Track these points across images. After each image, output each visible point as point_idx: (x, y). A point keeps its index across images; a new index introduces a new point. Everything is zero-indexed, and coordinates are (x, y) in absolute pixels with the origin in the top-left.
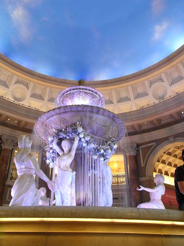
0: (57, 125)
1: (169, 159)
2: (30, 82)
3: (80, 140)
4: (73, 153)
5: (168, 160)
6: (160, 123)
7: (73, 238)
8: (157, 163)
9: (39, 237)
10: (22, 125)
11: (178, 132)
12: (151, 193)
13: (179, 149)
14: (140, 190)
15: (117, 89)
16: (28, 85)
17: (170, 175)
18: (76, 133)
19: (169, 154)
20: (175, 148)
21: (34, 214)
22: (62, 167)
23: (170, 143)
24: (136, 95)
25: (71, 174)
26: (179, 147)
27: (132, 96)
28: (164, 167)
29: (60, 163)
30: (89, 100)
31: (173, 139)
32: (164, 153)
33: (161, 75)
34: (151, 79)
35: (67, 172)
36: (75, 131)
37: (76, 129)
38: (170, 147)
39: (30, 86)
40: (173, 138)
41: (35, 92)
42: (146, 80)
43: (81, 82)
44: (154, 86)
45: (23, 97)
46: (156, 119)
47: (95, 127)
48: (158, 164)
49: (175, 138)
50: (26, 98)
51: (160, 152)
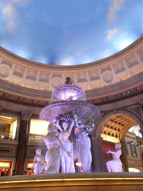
0: (59, 112)
1: (115, 125)
2: (13, 63)
3: (75, 122)
4: (70, 131)
5: (111, 124)
6: (108, 100)
7: (109, 187)
8: (104, 127)
9: (94, 187)
10: (6, 96)
11: (119, 107)
12: (114, 154)
13: (119, 118)
14: (109, 153)
15: (78, 73)
16: (11, 65)
17: (107, 134)
18: (73, 118)
19: (112, 121)
20: (116, 117)
21: (93, 177)
22: (65, 140)
23: (114, 114)
24: (91, 78)
25: (70, 144)
26: (119, 116)
27: (88, 79)
28: (108, 130)
29: (63, 137)
30: (76, 93)
31: (116, 111)
32: (109, 120)
33: (110, 66)
34: (103, 68)
35: (68, 143)
36: (72, 117)
37: (73, 116)
38: (113, 116)
39: (13, 66)
40: (116, 111)
41: (16, 71)
42: (100, 68)
43: (68, 79)
44: (104, 73)
45: (6, 75)
46: (105, 97)
47: (83, 113)
48: (104, 128)
49: (117, 111)
50: (10, 75)
51: (107, 121)
